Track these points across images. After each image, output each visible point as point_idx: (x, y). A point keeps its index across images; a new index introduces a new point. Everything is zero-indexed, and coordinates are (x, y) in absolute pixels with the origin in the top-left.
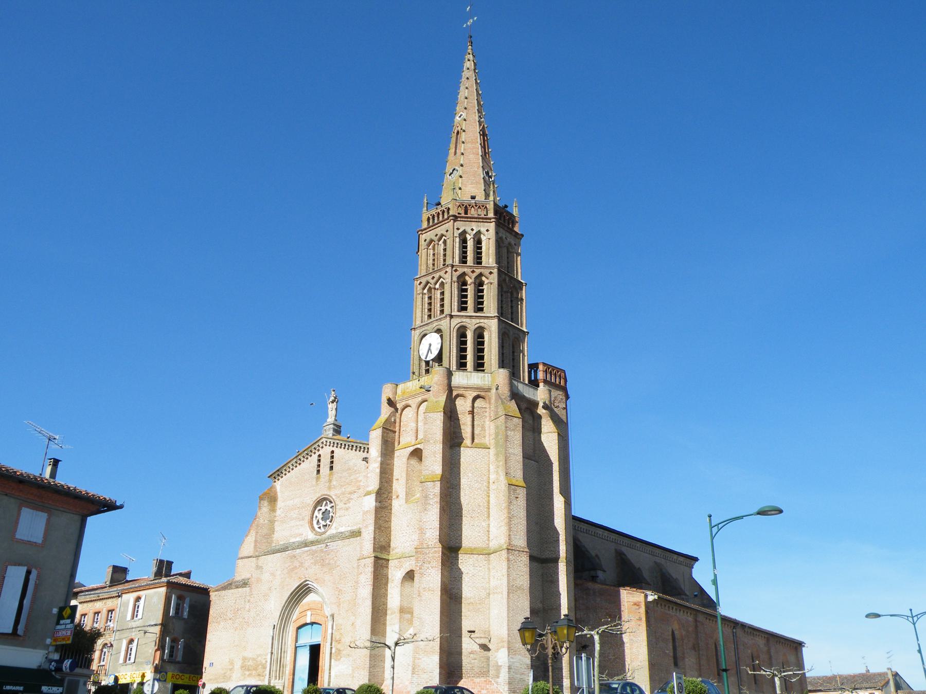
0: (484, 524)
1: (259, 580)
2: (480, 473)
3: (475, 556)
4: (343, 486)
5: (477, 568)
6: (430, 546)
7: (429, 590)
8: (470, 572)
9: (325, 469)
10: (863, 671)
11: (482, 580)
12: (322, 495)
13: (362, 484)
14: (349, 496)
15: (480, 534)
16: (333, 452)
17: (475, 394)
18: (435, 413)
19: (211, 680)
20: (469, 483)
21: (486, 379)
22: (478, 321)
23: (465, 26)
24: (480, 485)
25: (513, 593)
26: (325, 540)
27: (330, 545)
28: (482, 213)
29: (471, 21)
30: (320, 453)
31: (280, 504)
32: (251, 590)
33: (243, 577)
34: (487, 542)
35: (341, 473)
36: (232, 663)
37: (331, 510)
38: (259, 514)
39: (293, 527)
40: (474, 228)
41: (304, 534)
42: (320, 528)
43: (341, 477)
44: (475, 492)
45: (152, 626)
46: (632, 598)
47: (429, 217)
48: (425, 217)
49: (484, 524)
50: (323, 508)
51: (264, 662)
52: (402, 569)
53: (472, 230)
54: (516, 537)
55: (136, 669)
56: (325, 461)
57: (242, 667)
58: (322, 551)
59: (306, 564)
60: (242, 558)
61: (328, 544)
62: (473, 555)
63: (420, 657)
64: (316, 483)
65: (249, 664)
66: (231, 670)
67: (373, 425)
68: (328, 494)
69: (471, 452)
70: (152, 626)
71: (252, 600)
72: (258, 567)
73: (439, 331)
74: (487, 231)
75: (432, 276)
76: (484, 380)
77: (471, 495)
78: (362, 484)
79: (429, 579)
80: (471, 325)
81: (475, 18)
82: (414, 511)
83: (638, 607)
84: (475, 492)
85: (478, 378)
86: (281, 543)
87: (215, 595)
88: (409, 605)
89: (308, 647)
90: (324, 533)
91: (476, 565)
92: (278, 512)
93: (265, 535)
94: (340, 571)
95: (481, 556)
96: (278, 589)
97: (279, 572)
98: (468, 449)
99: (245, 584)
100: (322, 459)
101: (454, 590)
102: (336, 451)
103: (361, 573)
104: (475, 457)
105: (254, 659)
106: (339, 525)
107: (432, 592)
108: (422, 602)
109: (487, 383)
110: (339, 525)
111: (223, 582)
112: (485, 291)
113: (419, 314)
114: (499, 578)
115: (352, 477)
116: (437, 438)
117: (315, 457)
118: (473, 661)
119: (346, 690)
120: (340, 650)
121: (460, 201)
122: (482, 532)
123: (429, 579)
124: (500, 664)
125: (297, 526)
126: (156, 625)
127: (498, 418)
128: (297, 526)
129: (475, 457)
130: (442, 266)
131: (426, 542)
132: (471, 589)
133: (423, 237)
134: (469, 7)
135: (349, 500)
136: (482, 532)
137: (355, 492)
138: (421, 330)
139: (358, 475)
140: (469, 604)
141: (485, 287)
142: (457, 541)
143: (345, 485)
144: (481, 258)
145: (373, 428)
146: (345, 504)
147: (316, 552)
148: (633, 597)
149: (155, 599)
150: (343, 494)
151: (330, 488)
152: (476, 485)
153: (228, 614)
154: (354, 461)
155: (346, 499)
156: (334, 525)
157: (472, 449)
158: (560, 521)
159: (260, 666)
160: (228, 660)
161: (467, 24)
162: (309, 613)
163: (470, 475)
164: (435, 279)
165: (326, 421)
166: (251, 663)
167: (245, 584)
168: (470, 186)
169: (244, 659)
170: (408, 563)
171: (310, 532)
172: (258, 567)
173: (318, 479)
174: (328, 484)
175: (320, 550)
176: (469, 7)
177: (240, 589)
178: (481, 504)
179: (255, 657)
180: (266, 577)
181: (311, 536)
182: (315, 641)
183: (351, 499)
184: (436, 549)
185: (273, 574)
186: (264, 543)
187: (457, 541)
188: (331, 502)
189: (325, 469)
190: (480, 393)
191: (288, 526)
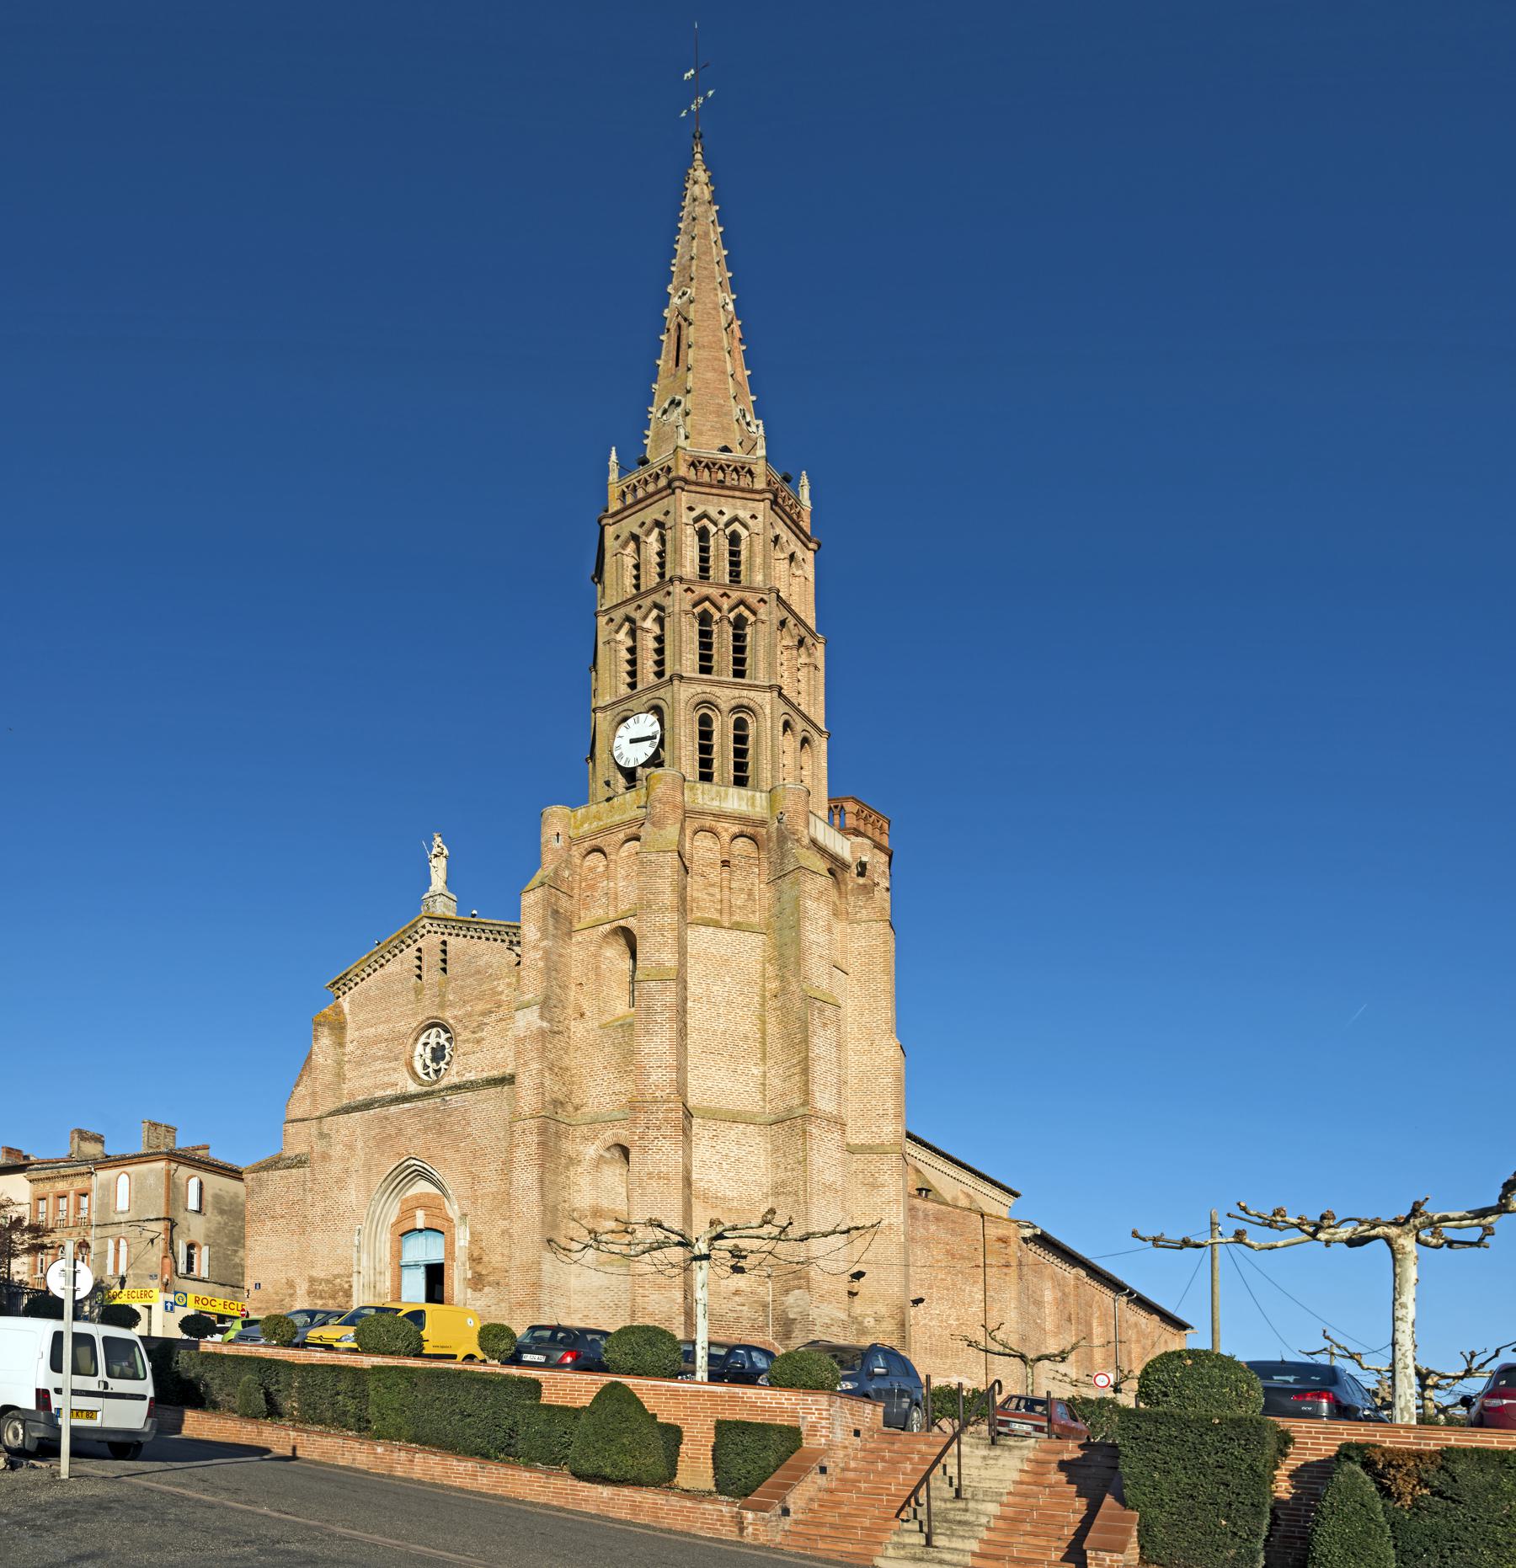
0: (755, 1071)
1: (325, 1157)
2: (747, 977)
3: (742, 1126)
4: (468, 1002)
5: (744, 1148)
6: (659, 1099)
7: (660, 1178)
8: (732, 1154)
9: (432, 975)
10: (1280, 1360)
11: (755, 1169)
12: (428, 1019)
13: (504, 997)
14: (481, 1018)
15: (748, 1089)
16: (444, 943)
17: (736, 829)
18: (661, 854)
19: (260, 1308)
20: (726, 994)
21: (758, 802)
22: (736, 693)
23: (683, 115)
24: (748, 1000)
25: (818, 1195)
26: (442, 1090)
27: (451, 1100)
28: (745, 481)
29: (700, 100)
30: (420, 944)
31: (351, 1033)
32: (312, 1172)
33: (297, 1152)
34: (761, 1103)
35: (463, 980)
36: (291, 1284)
37: (447, 1045)
38: (315, 1048)
39: (379, 1071)
40: (724, 510)
41: (400, 1084)
42: (427, 1074)
43: (462, 987)
44: (738, 1011)
45: (152, 1220)
46: (995, 1230)
47: (624, 492)
48: (614, 491)
49: (755, 1071)
50: (433, 1042)
51: (346, 1286)
52: (597, 1142)
53: (721, 513)
54: (823, 1095)
55: (135, 1284)
56: (432, 959)
57: (309, 1293)
58: (436, 1110)
59: (409, 1131)
60: (293, 1121)
61: (448, 1098)
62: (736, 1125)
63: (647, 1293)
64: (417, 997)
65: (321, 1288)
66: (291, 1295)
67: (526, 884)
68: (441, 1016)
69: (728, 938)
70: (152, 1220)
71: (316, 1188)
72: (322, 1135)
73: (657, 710)
74: (754, 517)
75: (639, 603)
76: (753, 805)
77: (730, 1017)
78: (504, 997)
79: (658, 1157)
80: (726, 697)
81: (710, 93)
82: (616, 1041)
83: (1004, 1245)
84: (738, 1011)
85: (740, 799)
86: (360, 1098)
87: (253, 1179)
88: (613, 1206)
89: (423, 1269)
90: (436, 1082)
91: (744, 1142)
92: (349, 1048)
93: (330, 1084)
94: (473, 1144)
95: (752, 1126)
96: (361, 1172)
97: (360, 1144)
98: (723, 931)
99: (300, 1162)
100: (425, 957)
101: (702, 1184)
102: (451, 940)
103: (518, 1145)
104: (738, 947)
105: (328, 1281)
106: (465, 1069)
107: (666, 1182)
108: (646, 1198)
109: (758, 809)
110: (465, 1069)
111: (264, 1156)
112: (748, 639)
113: (610, 682)
114: (789, 1167)
115: (485, 987)
116: (666, 901)
117: (411, 952)
118: (741, 1308)
119: (77, 1298)
120: (480, 1275)
121: (693, 453)
122: (752, 1084)
123: (658, 1157)
124: (791, 1316)
125: (385, 1070)
126: (157, 1219)
127: (784, 875)
128: (385, 1070)
129: (738, 947)
130: (624, 690)
131: (650, 1091)
132: (734, 1184)
133: (610, 531)
134: (692, 72)
135: (481, 1026)
136: (752, 1084)
137: (491, 1012)
138: (616, 711)
139: (495, 983)
140: (730, 1209)
141: (748, 630)
142: (705, 1097)
143: (472, 1000)
144: (738, 574)
145: (528, 888)
146: (474, 1032)
147: (425, 1111)
148: (997, 1228)
149: (151, 1181)
150: (470, 1015)
151: (442, 1006)
152: (740, 999)
153: (278, 1208)
154: (485, 958)
155: (475, 1024)
156: (454, 1068)
157: (731, 931)
158: (891, 1080)
159: (341, 1294)
160: (284, 1281)
161: (689, 110)
162: (420, 1213)
163: (728, 979)
164: (643, 610)
165: (428, 891)
166: (323, 1287)
167: (300, 1162)
168: (710, 433)
169: (312, 1280)
170: (609, 1133)
171: (410, 1081)
172: (322, 1135)
173: (418, 991)
174: (437, 1000)
175: (433, 1108)
176: (692, 72)
177: (294, 1171)
178: (750, 1035)
179: (329, 1277)
180: (337, 1151)
181: (413, 1088)
182: (436, 1255)
183: (485, 1024)
184: (671, 1105)
185: (351, 1147)
186: (329, 1096)
187: (705, 1097)
188: (447, 1031)
189: (432, 975)
190: (745, 828)
191: (369, 1070)
